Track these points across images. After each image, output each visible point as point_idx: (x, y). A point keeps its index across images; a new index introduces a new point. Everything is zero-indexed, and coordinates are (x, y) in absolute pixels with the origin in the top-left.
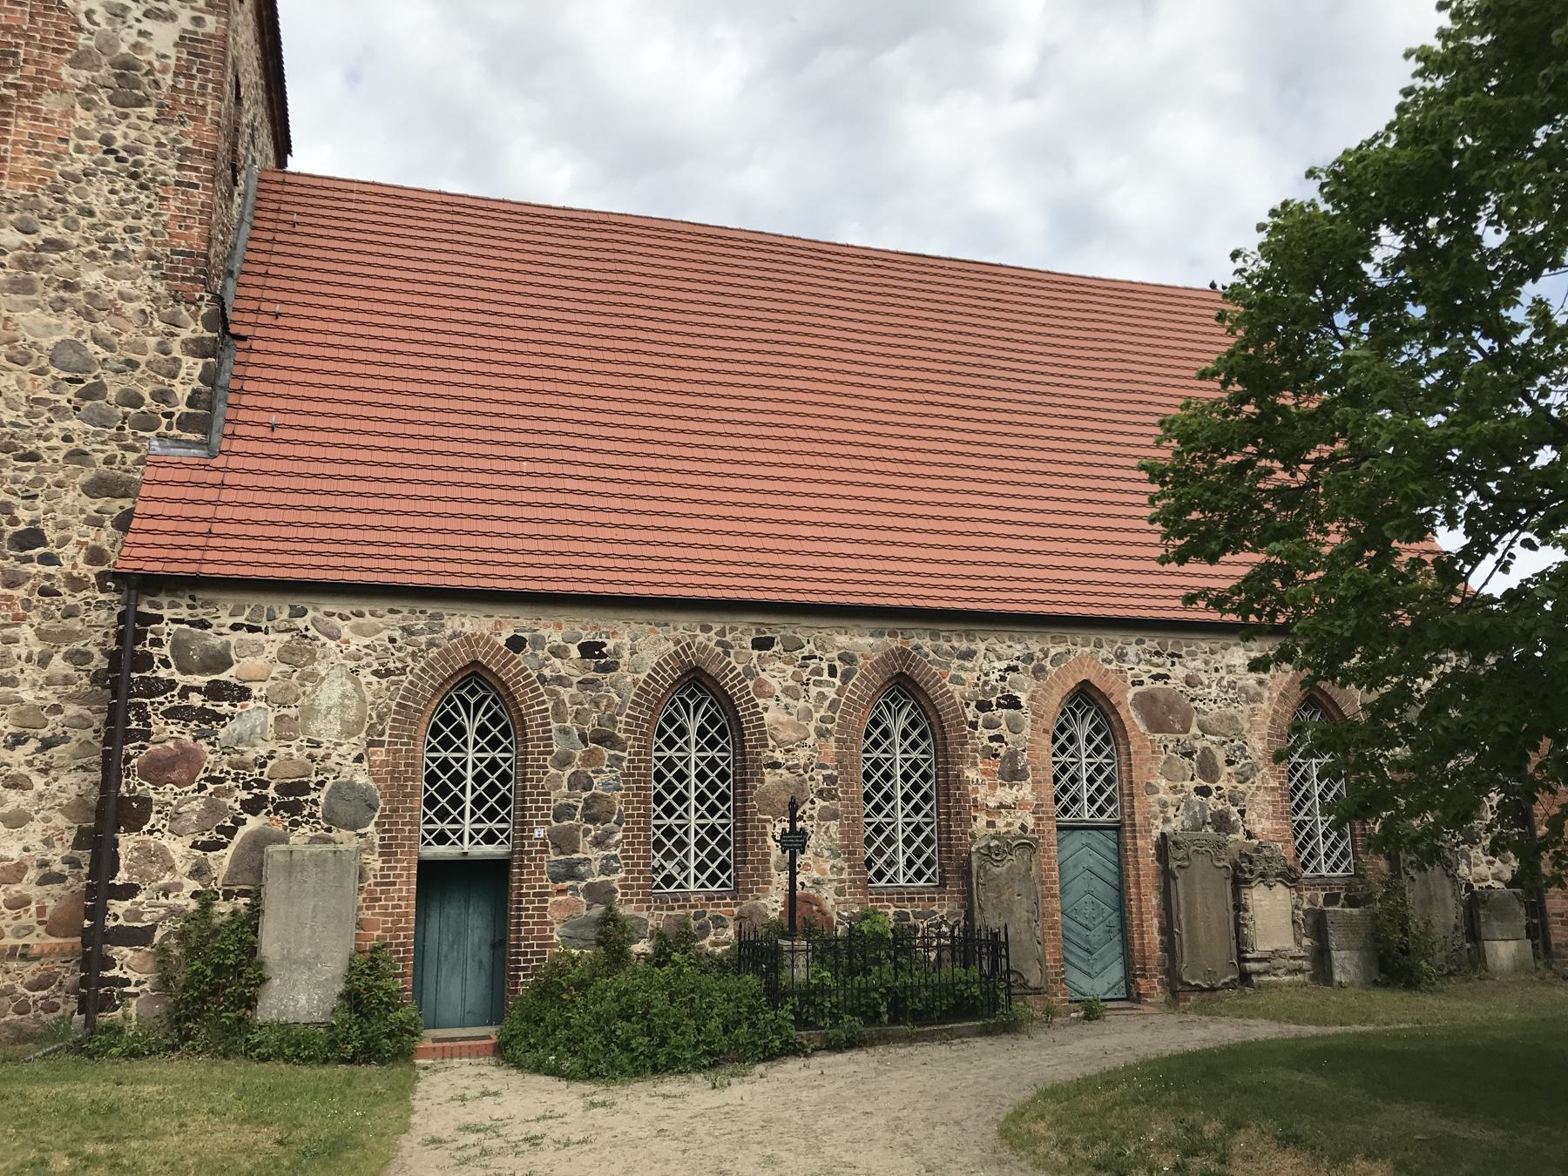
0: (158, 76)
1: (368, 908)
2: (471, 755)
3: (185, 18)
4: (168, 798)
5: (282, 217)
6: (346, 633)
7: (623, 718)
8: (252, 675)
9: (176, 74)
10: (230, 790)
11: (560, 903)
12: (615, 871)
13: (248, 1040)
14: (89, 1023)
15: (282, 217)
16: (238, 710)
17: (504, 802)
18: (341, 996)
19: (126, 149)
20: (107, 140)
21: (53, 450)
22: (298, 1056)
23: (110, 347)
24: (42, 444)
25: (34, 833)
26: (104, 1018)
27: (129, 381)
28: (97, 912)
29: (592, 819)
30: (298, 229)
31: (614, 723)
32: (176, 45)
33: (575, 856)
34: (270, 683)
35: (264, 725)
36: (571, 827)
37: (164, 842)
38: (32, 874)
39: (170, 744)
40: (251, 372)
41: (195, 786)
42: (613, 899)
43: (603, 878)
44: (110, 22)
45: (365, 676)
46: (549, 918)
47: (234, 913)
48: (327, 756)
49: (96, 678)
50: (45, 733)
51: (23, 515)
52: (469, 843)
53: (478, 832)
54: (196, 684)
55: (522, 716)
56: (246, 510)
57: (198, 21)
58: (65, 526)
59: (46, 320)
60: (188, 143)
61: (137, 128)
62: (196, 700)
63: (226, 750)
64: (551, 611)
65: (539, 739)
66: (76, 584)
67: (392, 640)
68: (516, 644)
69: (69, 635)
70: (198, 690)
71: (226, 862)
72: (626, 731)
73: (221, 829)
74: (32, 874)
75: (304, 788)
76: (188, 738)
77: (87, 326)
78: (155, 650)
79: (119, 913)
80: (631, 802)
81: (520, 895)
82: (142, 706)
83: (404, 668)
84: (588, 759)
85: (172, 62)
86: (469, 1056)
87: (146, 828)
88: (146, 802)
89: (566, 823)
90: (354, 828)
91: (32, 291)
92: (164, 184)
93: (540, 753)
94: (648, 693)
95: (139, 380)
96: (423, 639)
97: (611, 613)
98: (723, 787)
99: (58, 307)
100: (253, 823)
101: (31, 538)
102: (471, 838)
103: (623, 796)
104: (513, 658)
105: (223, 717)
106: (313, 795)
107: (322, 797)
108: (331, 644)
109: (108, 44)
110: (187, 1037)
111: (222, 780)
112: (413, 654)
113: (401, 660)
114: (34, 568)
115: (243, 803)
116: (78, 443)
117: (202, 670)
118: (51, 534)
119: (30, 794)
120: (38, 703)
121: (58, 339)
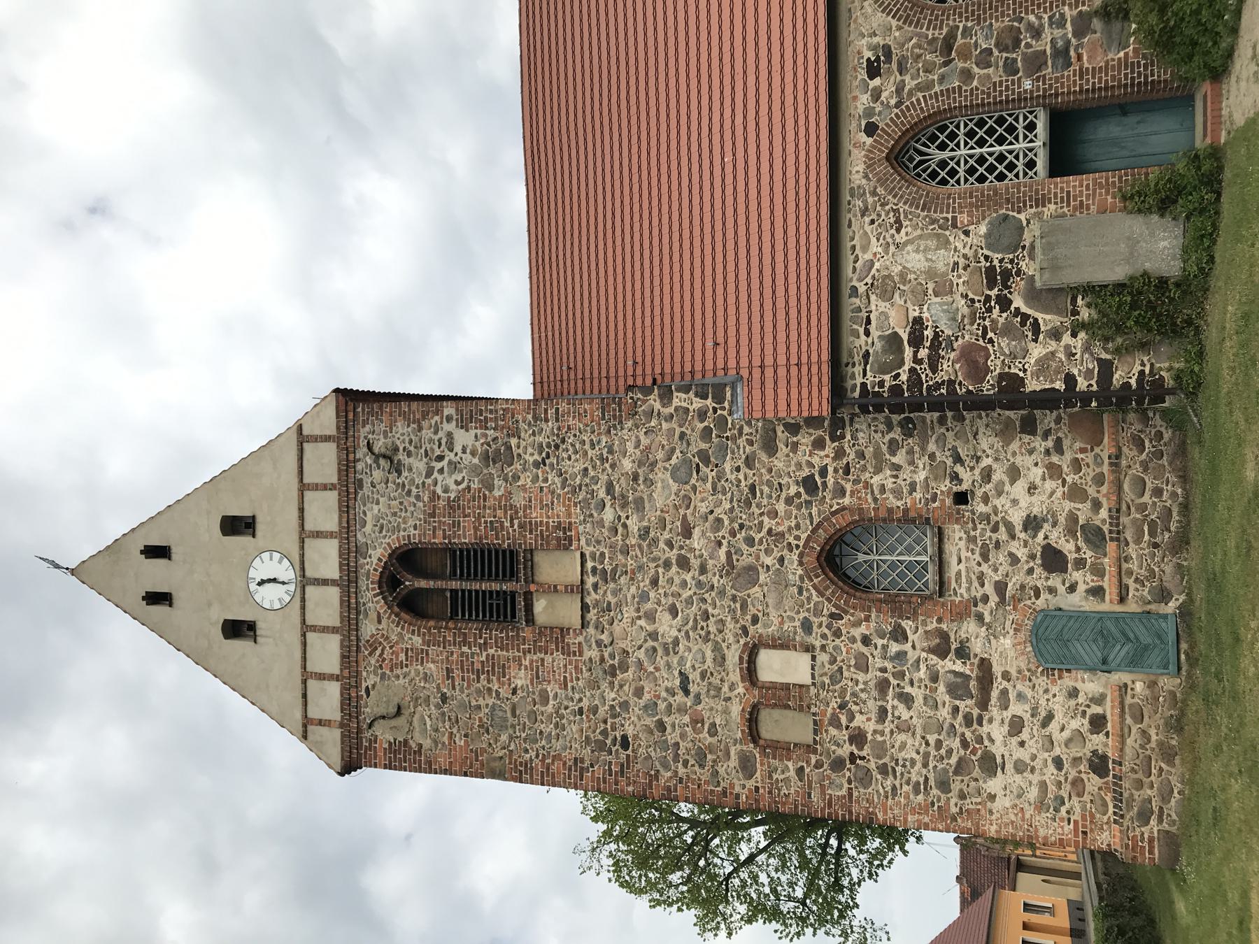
0: (489, 439)
1: (1088, 209)
2: (963, 151)
3: (450, 427)
4: (998, 362)
5: (565, 377)
6: (868, 256)
7: (930, 33)
8: (903, 317)
9: (487, 428)
10: (992, 321)
11: (1090, 58)
12: (1062, 15)
13: (1195, 276)
14: (1171, 392)
15: (565, 377)
16: (930, 324)
17: (1000, 121)
18: (1162, 216)
19: (540, 454)
20: (537, 465)
21: (746, 477)
22: (1211, 234)
23: (673, 450)
24: (743, 484)
25: (1023, 461)
26: (1169, 382)
27: (694, 437)
28: (1086, 398)
29: (1017, 43)
30: (572, 365)
31: (934, 39)
32: (467, 430)
33: (1048, 52)
34: (909, 304)
35: (941, 304)
36: (1023, 60)
37: (1032, 361)
38: (1055, 459)
39: (957, 366)
40: (677, 369)
41: (989, 346)
42: (1088, 13)
43: (1069, 25)
44: (460, 471)
45: (901, 237)
46: (1102, 64)
47: (1089, 306)
48: (965, 256)
49: (908, 434)
50: (949, 462)
51: (793, 490)
52: (1036, 143)
53: (1025, 137)
54: (911, 354)
55: (930, 115)
56: (781, 355)
57: (449, 419)
58: (799, 466)
59: (659, 489)
60: (530, 417)
61: (526, 448)
62: (923, 353)
63: (961, 327)
64: (843, 106)
65: (948, 98)
66: (840, 454)
67: (872, 222)
68: (871, 129)
69: (878, 454)
70: (915, 353)
71: (1048, 317)
72: (941, 28)
73: (1023, 324)
74: (1055, 459)
75: (990, 271)
76: (952, 355)
77: (660, 465)
78: (887, 385)
79: (1086, 384)
80: (1003, 12)
81: (1081, 91)
82: (929, 388)
83: (894, 211)
84: (965, 56)
85: (479, 432)
86: (1221, 102)
87: (1021, 374)
88: (1002, 376)
89: (1020, 64)
90: (1022, 228)
91: (642, 498)
92: (559, 429)
93: (960, 96)
94: (908, 15)
95: (693, 430)
96: (870, 200)
97: (842, 58)
98: (990, 122)
99: (650, 483)
100: (1018, 302)
101: (809, 484)
102: (1031, 141)
103: (997, 20)
104: (883, 130)
105: (936, 334)
106: (996, 263)
107: (996, 256)
108: (877, 265)
109: (474, 470)
110: (1189, 322)
111: (985, 328)
112: (883, 205)
113: (887, 213)
114: (830, 480)
115: (1002, 311)
116: (740, 463)
117: (902, 351)
118: (806, 472)
119: (995, 466)
120: (928, 468)
121: (671, 481)
